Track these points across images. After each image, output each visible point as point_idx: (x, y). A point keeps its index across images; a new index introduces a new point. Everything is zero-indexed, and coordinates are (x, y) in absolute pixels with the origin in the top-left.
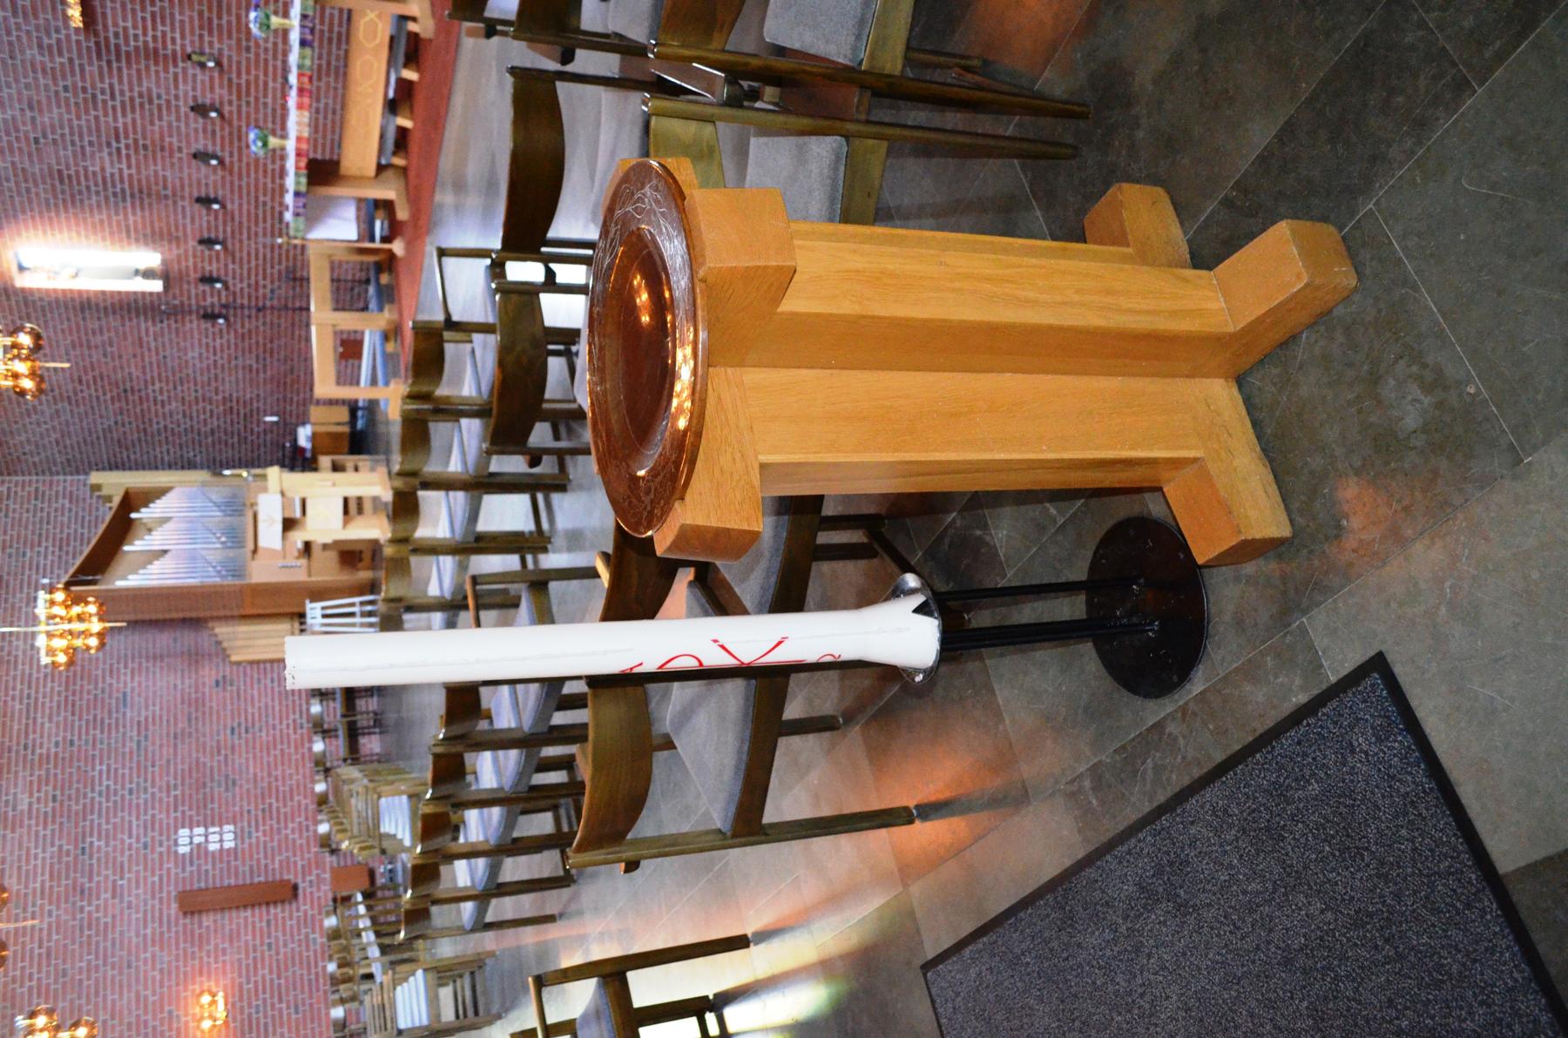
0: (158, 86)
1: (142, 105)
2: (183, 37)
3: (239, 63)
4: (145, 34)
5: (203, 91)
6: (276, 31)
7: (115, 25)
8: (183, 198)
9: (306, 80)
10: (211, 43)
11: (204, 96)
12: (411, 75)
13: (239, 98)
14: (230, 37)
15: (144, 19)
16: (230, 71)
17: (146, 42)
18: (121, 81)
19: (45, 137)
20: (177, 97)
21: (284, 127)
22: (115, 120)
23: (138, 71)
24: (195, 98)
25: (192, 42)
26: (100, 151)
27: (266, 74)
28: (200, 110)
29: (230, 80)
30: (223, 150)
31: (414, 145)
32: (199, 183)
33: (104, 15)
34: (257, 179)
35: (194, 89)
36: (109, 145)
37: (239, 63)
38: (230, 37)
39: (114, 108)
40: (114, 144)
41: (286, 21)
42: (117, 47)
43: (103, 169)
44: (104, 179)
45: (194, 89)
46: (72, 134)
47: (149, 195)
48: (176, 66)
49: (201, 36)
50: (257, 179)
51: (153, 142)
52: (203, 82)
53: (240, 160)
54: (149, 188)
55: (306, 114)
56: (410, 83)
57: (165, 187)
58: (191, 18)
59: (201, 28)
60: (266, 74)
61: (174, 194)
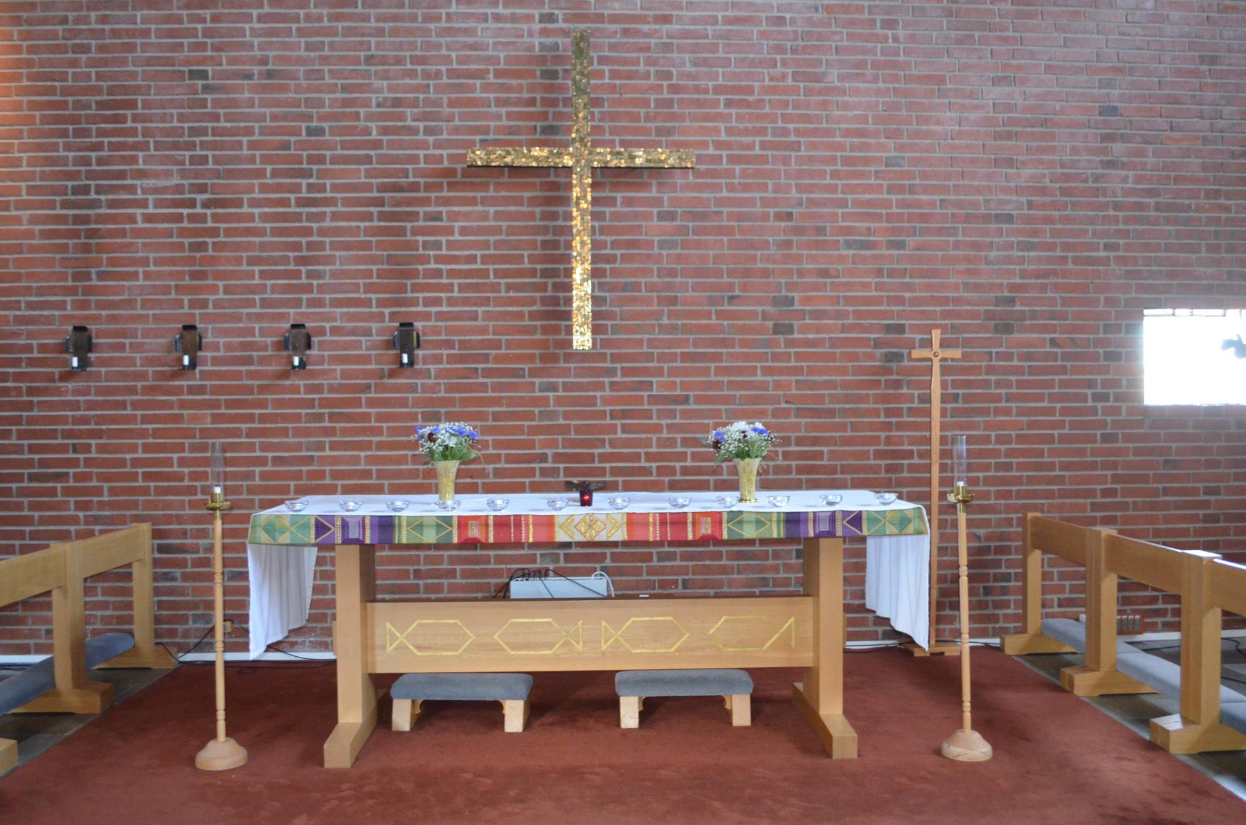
0: (334, 275)
1: (296, 247)
2: (441, 316)
3: (403, 403)
4: (439, 259)
5: (335, 346)
6: (734, 471)
7: (453, 217)
8: (84, 305)
9: (706, 529)
10: (437, 359)
11: (322, 345)
12: (514, 717)
13: (325, 403)
14: (451, 388)
15: (471, 259)
16: (381, 388)
17: (424, 259)
18: (336, 216)
19: (206, 89)
20: (320, 303)
21: (471, 489)
22: (254, 203)
23: (366, 246)
24: (322, 332)
25: (436, 331)
26: (183, 174)
27: (381, 446)
28: (299, 338)
29: (367, 388)
30: (204, 375)
31: (568, 746)
32: (123, 334)
33: (472, 202)
34: (142, 434)
35: (335, 331)
36: (202, 189)
37: (403, 403)
38: (451, 388)
39: (285, 203)
40: (200, 197)
41: (450, 487)
42: (413, 216)
43: (142, 174)
44: (121, 175)
45: (335, 331)
46: (215, 132)
47: (87, 248)
48: (382, 303)
49: (449, 344)
50: (142, 434)
51: (212, 260)
52: (357, 345)
53: (183, 405)
54: (100, 248)
55: (620, 535)
56: (500, 720)
57: (102, 276)
58: (483, 330)
59: (463, 345)
60: (381, 446)
61: (88, 291)
